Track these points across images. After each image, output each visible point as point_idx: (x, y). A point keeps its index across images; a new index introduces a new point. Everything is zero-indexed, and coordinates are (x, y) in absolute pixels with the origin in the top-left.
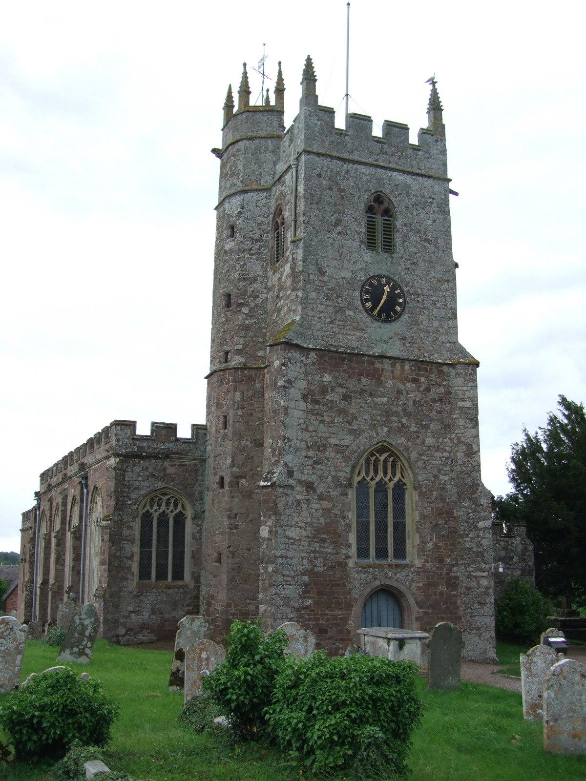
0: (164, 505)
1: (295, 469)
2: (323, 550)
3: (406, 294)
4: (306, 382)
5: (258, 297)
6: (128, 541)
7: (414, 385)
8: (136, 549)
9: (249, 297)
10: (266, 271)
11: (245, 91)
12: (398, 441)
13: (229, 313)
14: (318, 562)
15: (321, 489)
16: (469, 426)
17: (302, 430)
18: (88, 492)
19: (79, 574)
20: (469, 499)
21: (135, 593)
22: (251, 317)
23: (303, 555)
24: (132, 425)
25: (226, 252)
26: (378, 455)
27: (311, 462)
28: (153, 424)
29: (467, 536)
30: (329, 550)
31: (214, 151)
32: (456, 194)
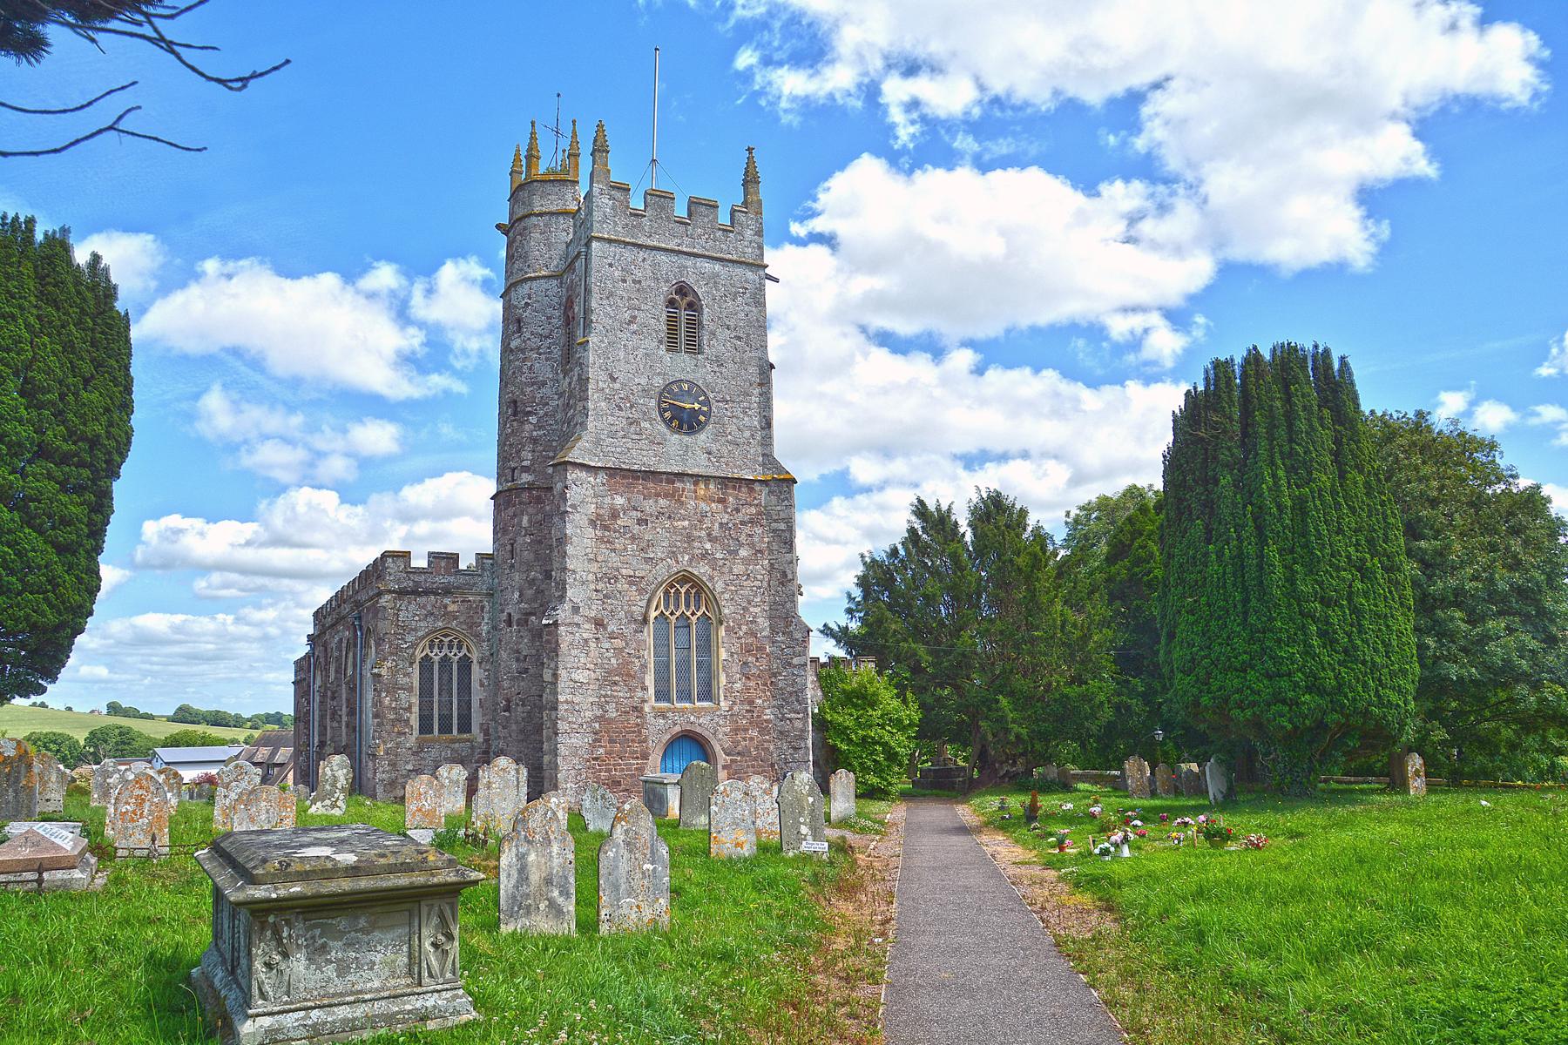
0: (445, 647)
4: (593, 506)
5: (548, 404)
7: (720, 506)
8: (415, 700)
9: (537, 405)
10: (557, 373)
11: (532, 157)
12: (701, 570)
13: (515, 424)
14: (611, 707)
15: (612, 628)
18: (362, 635)
19: (355, 730)
22: (540, 428)
23: (591, 699)
25: (512, 351)
29: (780, 674)
30: (621, 694)
31: (498, 227)
32: (776, 280)
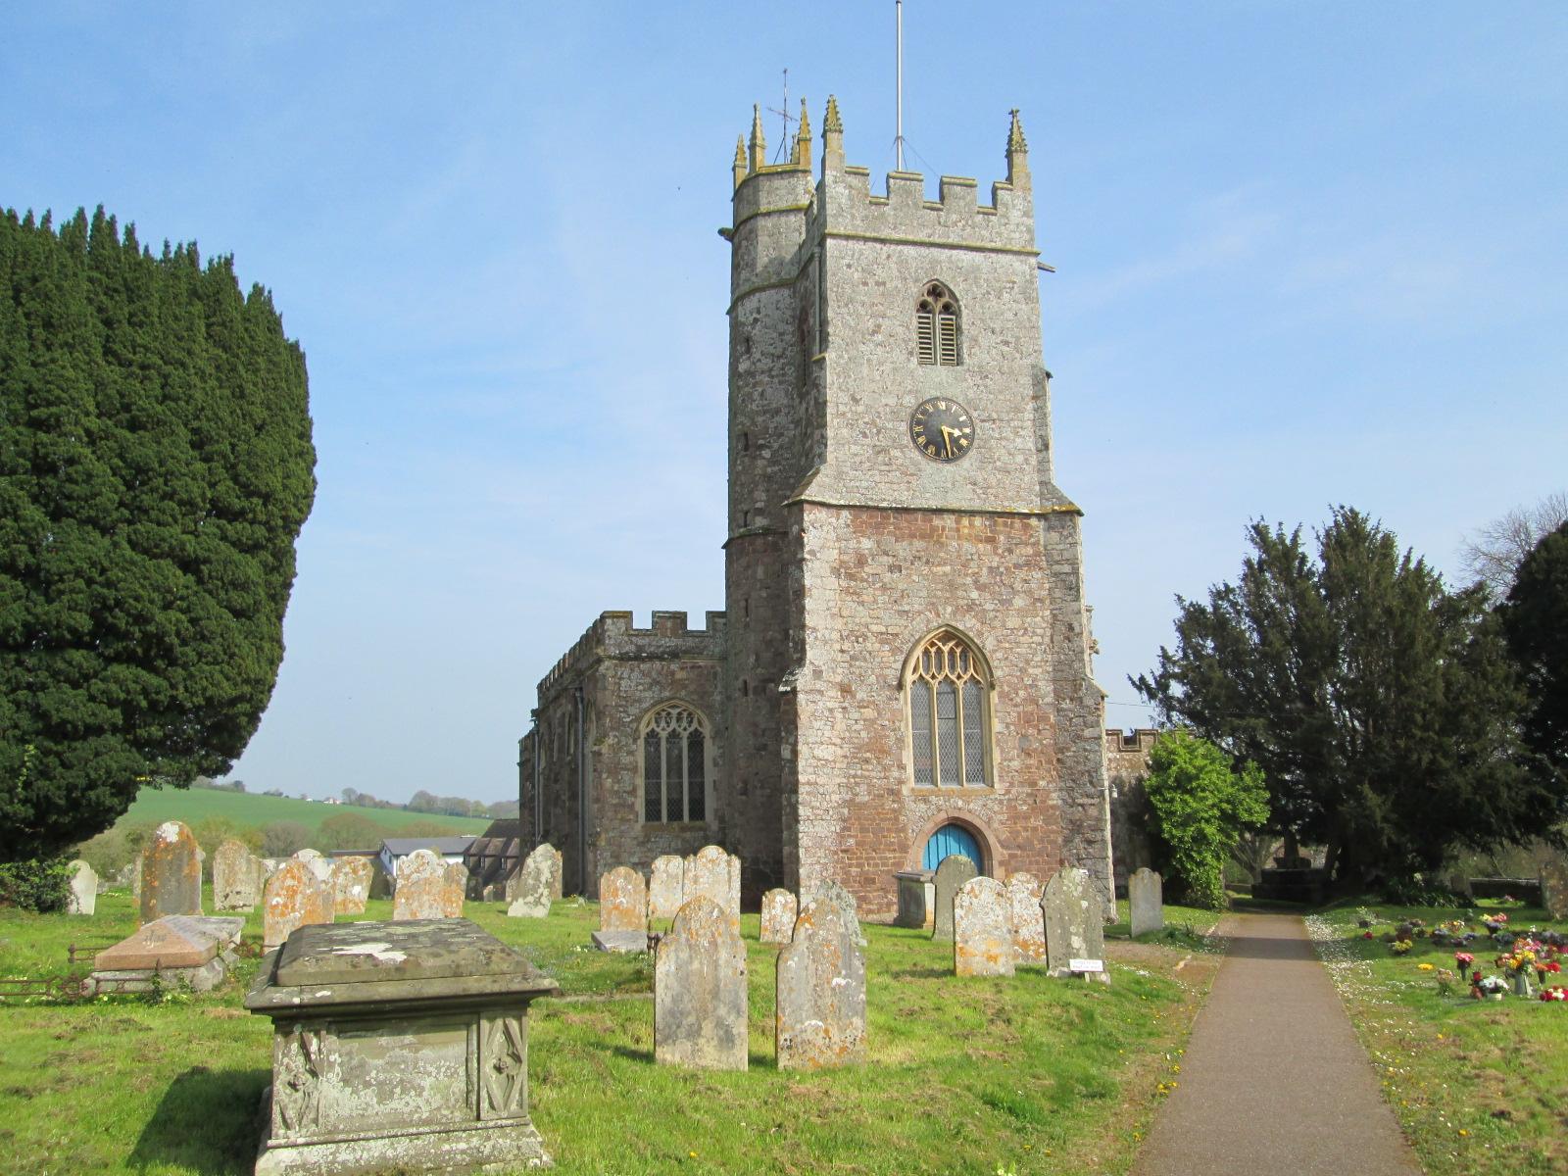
0: (674, 721)
1: (823, 668)
2: (867, 773)
3: (976, 421)
5: (782, 434)
6: (628, 770)
7: (989, 547)
9: (771, 436)
10: (792, 398)
13: (746, 460)
14: (862, 789)
16: (1069, 598)
17: (833, 616)
20: (1071, 700)
21: (641, 839)
24: (627, 616)
26: (940, 644)
27: (847, 657)
28: (654, 614)
30: (873, 774)
31: (722, 232)
